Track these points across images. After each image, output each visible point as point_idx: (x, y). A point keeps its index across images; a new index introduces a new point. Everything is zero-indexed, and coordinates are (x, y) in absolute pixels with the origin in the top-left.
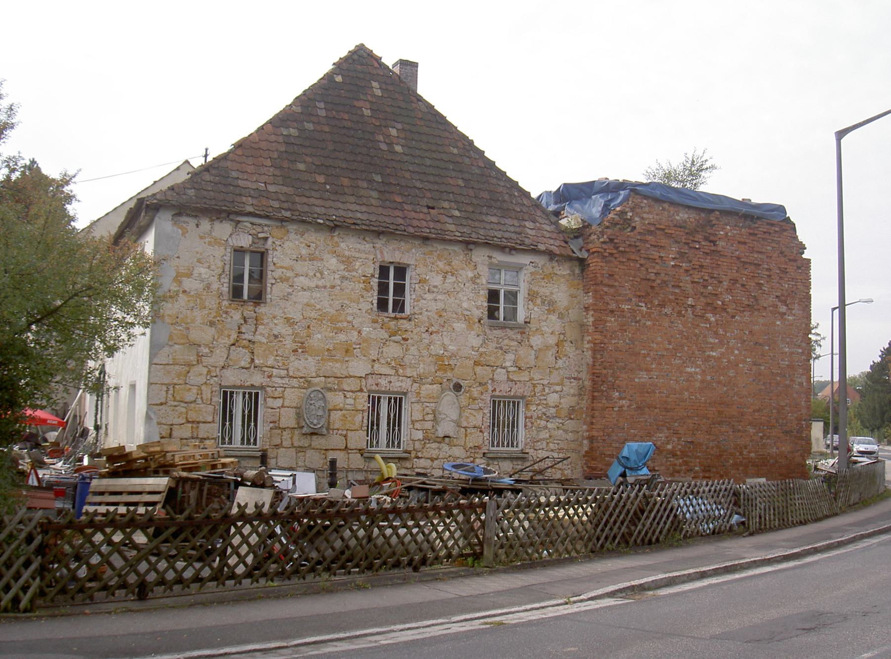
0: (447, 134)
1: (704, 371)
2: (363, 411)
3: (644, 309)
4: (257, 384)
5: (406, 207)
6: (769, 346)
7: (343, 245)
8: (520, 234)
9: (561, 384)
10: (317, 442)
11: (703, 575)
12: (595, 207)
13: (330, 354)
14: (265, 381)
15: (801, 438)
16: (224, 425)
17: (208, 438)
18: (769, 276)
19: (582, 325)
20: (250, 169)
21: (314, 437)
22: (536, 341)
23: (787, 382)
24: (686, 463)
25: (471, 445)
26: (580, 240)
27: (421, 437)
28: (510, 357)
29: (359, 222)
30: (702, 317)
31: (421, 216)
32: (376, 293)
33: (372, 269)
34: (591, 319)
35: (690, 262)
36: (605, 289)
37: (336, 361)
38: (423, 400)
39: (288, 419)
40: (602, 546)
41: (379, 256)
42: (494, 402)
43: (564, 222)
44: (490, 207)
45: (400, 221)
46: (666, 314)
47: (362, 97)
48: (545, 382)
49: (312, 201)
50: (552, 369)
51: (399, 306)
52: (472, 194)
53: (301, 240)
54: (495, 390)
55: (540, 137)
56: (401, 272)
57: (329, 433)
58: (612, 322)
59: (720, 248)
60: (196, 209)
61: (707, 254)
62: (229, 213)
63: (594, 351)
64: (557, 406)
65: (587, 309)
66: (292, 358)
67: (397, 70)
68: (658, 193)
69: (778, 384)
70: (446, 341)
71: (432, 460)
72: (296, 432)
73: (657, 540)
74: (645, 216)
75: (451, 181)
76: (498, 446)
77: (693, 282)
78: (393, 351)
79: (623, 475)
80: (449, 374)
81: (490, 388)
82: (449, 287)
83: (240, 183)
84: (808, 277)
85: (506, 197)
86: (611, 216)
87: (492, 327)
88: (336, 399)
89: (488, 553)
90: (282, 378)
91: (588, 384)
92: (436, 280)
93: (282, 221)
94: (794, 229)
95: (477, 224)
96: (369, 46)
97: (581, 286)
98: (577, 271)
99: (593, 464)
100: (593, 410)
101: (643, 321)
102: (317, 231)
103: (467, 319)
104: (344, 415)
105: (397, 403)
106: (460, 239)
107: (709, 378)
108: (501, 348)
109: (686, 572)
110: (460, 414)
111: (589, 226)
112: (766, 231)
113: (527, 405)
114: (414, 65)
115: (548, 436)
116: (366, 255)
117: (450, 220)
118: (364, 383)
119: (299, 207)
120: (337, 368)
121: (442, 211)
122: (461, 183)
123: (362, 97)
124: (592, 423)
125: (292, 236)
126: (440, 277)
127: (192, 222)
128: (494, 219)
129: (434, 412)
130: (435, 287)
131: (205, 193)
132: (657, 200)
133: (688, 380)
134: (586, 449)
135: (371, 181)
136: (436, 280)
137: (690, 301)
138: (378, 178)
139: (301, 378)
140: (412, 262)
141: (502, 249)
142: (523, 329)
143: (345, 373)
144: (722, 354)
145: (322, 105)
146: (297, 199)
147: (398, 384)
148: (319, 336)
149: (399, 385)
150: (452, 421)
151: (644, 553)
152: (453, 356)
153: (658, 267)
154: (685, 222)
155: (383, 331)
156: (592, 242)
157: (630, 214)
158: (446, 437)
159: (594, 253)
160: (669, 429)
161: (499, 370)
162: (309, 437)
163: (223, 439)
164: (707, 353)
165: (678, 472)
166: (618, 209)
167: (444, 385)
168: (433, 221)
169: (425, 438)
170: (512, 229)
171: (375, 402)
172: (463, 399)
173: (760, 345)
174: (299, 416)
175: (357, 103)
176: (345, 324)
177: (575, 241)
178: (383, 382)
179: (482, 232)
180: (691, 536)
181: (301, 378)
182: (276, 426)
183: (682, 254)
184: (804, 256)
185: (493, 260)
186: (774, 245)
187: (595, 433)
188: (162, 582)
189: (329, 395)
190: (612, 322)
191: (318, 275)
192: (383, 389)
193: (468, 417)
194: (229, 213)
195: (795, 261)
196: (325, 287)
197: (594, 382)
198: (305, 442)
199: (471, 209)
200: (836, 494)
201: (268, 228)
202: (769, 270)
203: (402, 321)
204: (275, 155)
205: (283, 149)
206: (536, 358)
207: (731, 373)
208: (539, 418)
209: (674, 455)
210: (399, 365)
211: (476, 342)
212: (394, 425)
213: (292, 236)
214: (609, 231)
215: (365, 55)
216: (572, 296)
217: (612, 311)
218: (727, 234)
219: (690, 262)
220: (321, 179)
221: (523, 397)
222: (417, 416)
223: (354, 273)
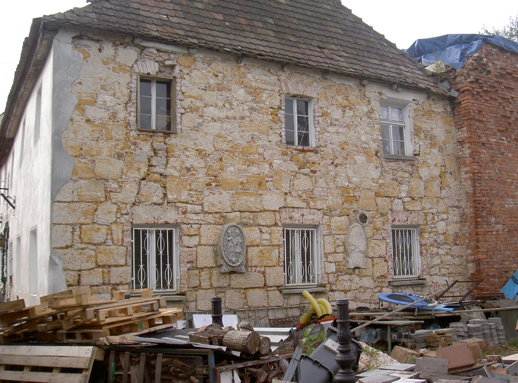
2: (279, 246)
3: (506, 142)
4: (171, 221)
7: (250, 76)
10: (236, 281)
16: (137, 268)
17: (121, 284)
21: (233, 276)
22: (424, 172)
25: (378, 274)
27: (334, 270)
29: (263, 53)
31: (317, 54)
32: (283, 126)
34: (468, 152)
36: (477, 124)
37: (251, 195)
38: (334, 232)
39: (206, 257)
42: (393, 231)
48: (434, 211)
49: (215, 33)
51: (304, 140)
54: (394, 220)
56: (305, 102)
57: (247, 271)
58: (485, 154)
66: (206, 193)
68: (502, 43)
70: (350, 174)
71: (345, 292)
72: (215, 272)
74: (496, 62)
76: (399, 274)
78: (303, 183)
80: (355, 206)
83: (142, 13)
85: (379, 46)
86: (470, 61)
88: (252, 234)
90: (197, 214)
91: (469, 211)
92: (337, 114)
95: (364, 64)
97: (453, 123)
98: (449, 109)
101: (506, 154)
102: (224, 61)
103: (366, 152)
104: (261, 251)
105: (308, 234)
108: (396, 180)
110: (367, 245)
116: (271, 86)
120: (249, 201)
124: (478, 247)
125: (199, 65)
126: (340, 111)
130: (337, 120)
138: (271, 21)
139: (216, 213)
140: (315, 95)
142: (412, 161)
143: (260, 207)
146: (201, 31)
147: (310, 217)
148: (232, 169)
149: (310, 218)
150: (361, 252)
153: (511, 106)
155: (292, 164)
159: (463, 92)
161: (396, 201)
162: (227, 276)
163: (138, 283)
169: (337, 271)
171: (288, 235)
174: (216, 254)
176: (257, 156)
178: (296, 215)
181: (216, 213)
182: (194, 266)
185: (383, 97)
187: (481, 256)
190: (485, 154)
191: (227, 105)
192: (297, 222)
193: (374, 248)
196: (235, 118)
198: (224, 282)
201: (176, 56)
203: (309, 154)
206: (425, 189)
208: (432, 245)
210: (309, 197)
211: (375, 174)
213: (199, 65)
216: (448, 132)
217: (483, 144)
220: (220, 17)
221: (416, 226)
222: (330, 248)
223: (262, 105)
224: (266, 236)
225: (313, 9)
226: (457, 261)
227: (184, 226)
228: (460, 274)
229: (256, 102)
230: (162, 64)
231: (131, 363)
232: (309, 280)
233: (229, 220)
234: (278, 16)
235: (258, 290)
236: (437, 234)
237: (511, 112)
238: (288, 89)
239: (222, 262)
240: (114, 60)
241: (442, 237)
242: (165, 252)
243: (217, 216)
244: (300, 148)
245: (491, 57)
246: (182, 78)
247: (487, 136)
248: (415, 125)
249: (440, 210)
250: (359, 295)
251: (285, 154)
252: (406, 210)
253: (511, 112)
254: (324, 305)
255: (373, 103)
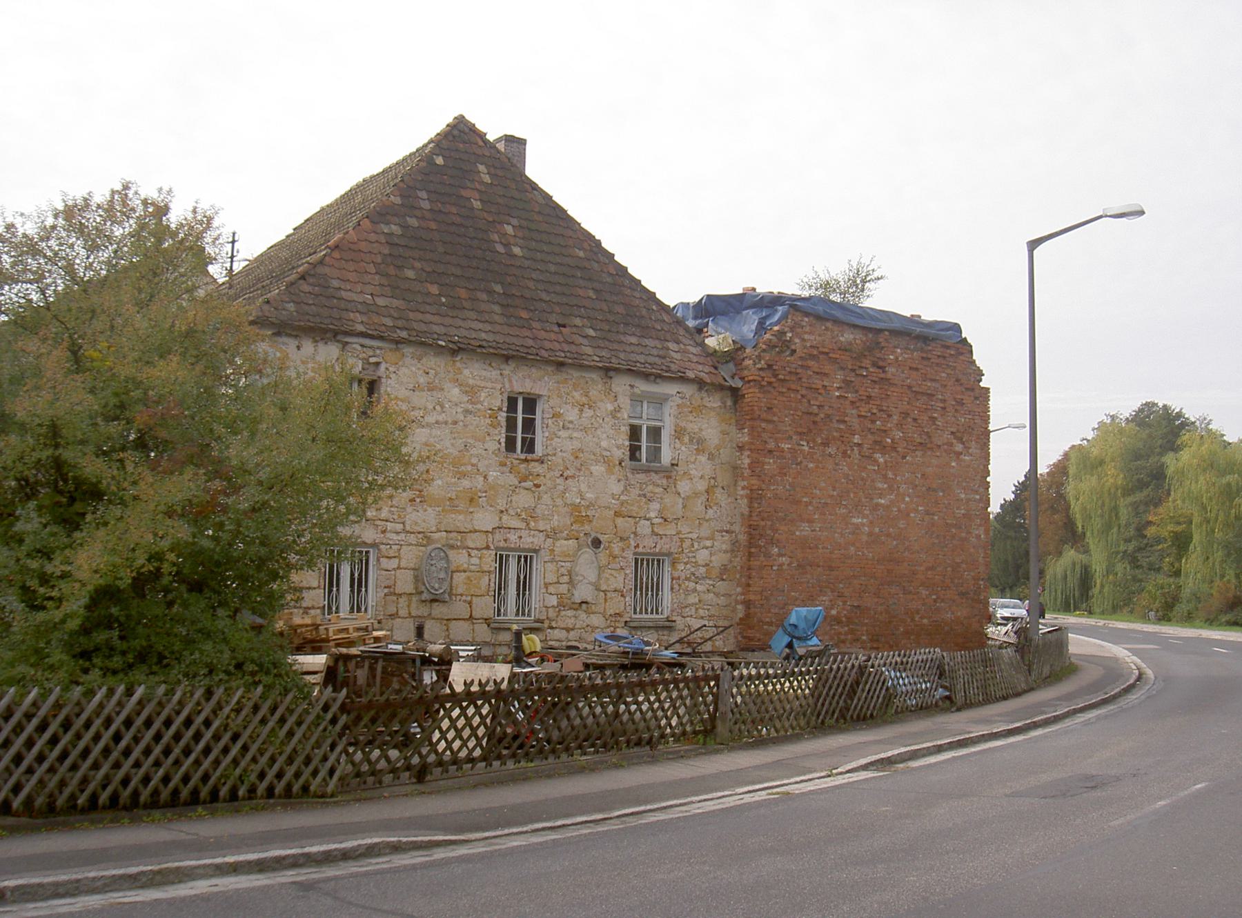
0: (570, 233)
1: (871, 522)
3: (806, 448)
4: (369, 541)
5: (535, 325)
6: (943, 491)
7: (466, 372)
8: (664, 358)
9: (712, 538)
10: (438, 610)
11: (939, 749)
12: (748, 326)
13: (451, 505)
14: (378, 537)
15: (980, 602)
16: (330, 591)
17: (313, 608)
18: (944, 408)
19: (735, 468)
20: (352, 276)
22: (684, 487)
23: (963, 535)
24: (852, 631)
25: (612, 612)
26: (731, 365)
27: (555, 603)
28: (655, 506)
29: (484, 344)
30: (869, 457)
31: (553, 336)
32: (504, 430)
33: (499, 401)
34: (747, 461)
35: (857, 392)
36: (763, 425)
37: (460, 512)
38: (557, 558)
39: (405, 583)
40: (823, 722)
41: (507, 386)
42: (636, 560)
43: (711, 342)
44: (626, 324)
45: (530, 342)
46: (830, 455)
47: (469, 184)
48: (694, 536)
49: (428, 317)
50: (702, 520)
51: (529, 446)
52: (605, 308)
53: (419, 365)
54: (638, 546)
55: (681, 235)
56: (531, 404)
58: (770, 464)
59: (889, 376)
60: (300, 329)
61: (875, 382)
62: (336, 334)
63: (751, 500)
64: (707, 565)
65: (741, 448)
66: (409, 509)
67: (501, 146)
68: (820, 309)
69: (953, 537)
70: (583, 487)
71: (568, 630)
72: (414, 599)
73: (872, 715)
74: (806, 337)
75: (581, 292)
76: (641, 613)
77: (859, 416)
78: (523, 499)
79: (790, 646)
80: (587, 528)
81: (633, 544)
82: (585, 421)
83: (344, 294)
84: (987, 409)
85: (644, 312)
86: (768, 336)
87: (635, 471)
88: (459, 558)
89: (721, 728)
90: (397, 533)
91: (743, 538)
92: (572, 414)
93: (397, 342)
94: (971, 352)
95: (615, 346)
96: (470, 118)
97: (733, 421)
98: (729, 403)
99: (750, 633)
100: (749, 569)
101: (805, 463)
102: (437, 354)
103: (607, 461)
104: (468, 578)
105: (526, 561)
106: (600, 365)
107: (877, 530)
108: (645, 496)
109: (925, 745)
111: (742, 348)
112: (938, 354)
113: (674, 564)
114: (522, 142)
115: (695, 604)
116: (491, 384)
117: (585, 341)
118: (490, 539)
119: (415, 325)
120: (459, 521)
121: (574, 330)
122: (591, 294)
123: (469, 184)
124: (749, 585)
125: (408, 360)
126: (576, 410)
127: (292, 343)
128: (634, 340)
129: (570, 573)
130: (571, 422)
131: (306, 307)
132: (819, 318)
133: (853, 533)
134: (741, 615)
135: (490, 292)
136: (572, 414)
137: (857, 439)
138: (498, 288)
140: (544, 392)
141: (646, 376)
142: (669, 472)
143: (469, 527)
144: (892, 501)
145: (424, 195)
146: (411, 315)
147: (530, 540)
148: (440, 482)
149: (529, 540)
150: (590, 583)
151: (861, 729)
152: (591, 505)
153: (821, 398)
154: (850, 344)
155: (512, 476)
156: (746, 368)
157: (789, 335)
158: (583, 606)
159: (749, 382)
160: (833, 591)
161: (642, 522)
163: (330, 608)
164: (875, 501)
165: (843, 642)
166: (776, 328)
167: (581, 541)
168: (566, 342)
169: (559, 604)
170: (655, 352)
171: (502, 561)
172: (603, 556)
173: (934, 490)
174: (417, 579)
175: (463, 193)
176: (469, 468)
177: (724, 367)
178: (513, 537)
179: (622, 356)
180: (902, 712)
182: (391, 592)
183: (847, 383)
184: (982, 384)
185: (636, 390)
186: (949, 371)
187: (752, 597)
188: (440, 763)
189: (452, 554)
190: (770, 464)
191: (438, 408)
194: (336, 334)
195: (973, 390)
196: (446, 423)
197: (751, 536)
199: (607, 328)
200: (1029, 666)
201: (380, 351)
202: (944, 401)
203: (533, 464)
204: (379, 259)
205: (386, 251)
206: (684, 507)
207: (902, 524)
208: (687, 579)
209: (839, 623)
210: (530, 516)
211: (617, 488)
212: (524, 589)
213: (408, 360)
214: (767, 356)
215: (467, 130)
216: (724, 433)
217: (770, 451)
218: (897, 358)
219: (857, 392)
220: (434, 289)
221: (669, 554)
222: (551, 578)
223: (479, 406)
224: (475, 561)
225: (558, 259)
226: (722, 601)
227: (382, 547)
228: (726, 618)
229: (473, 403)
230: (366, 361)
231: (357, 667)
232: (523, 614)
233: (434, 542)
234: (509, 279)
235: (461, 622)
236: (696, 565)
237: (820, 407)
238: (511, 386)
239: (423, 588)
240: (313, 359)
241: (703, 570)
242: (360, 575)
243: (420, 536)
244: (523, 456)
245: (799, 330)
246: (388, 377)
247: (776, 440)
248: (677, 425)
249: (702, 534)
250: (584, 635)
251: (503, 464)
252: (654, 533)
253: (820, 407)
254: (533, 641)
255: (621, 399)
